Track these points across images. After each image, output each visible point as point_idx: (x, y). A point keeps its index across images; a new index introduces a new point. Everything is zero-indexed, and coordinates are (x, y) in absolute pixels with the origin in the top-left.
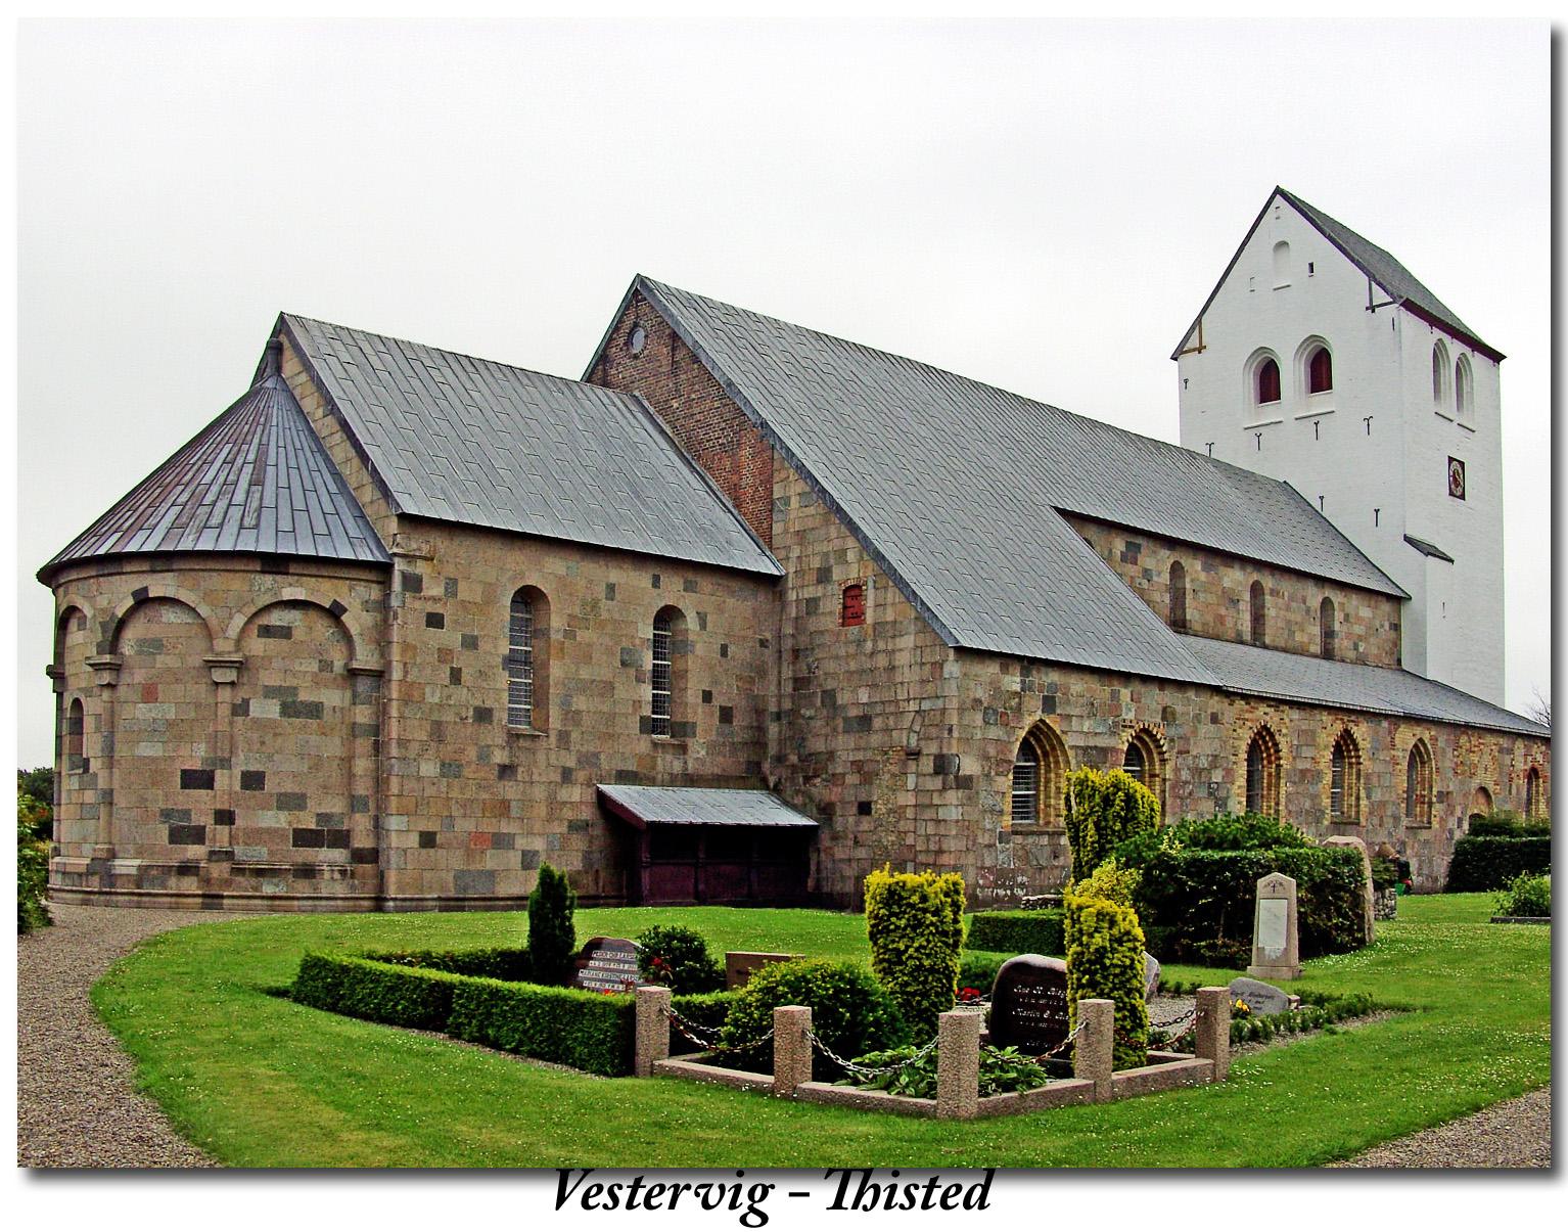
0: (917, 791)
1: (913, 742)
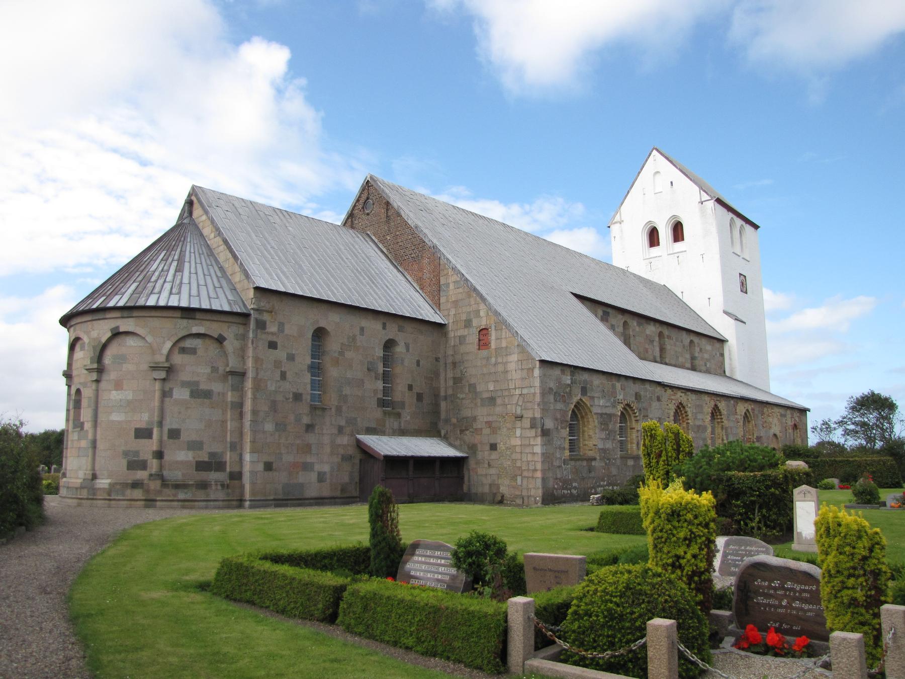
0: (521, 437)
1: (519, 412)
